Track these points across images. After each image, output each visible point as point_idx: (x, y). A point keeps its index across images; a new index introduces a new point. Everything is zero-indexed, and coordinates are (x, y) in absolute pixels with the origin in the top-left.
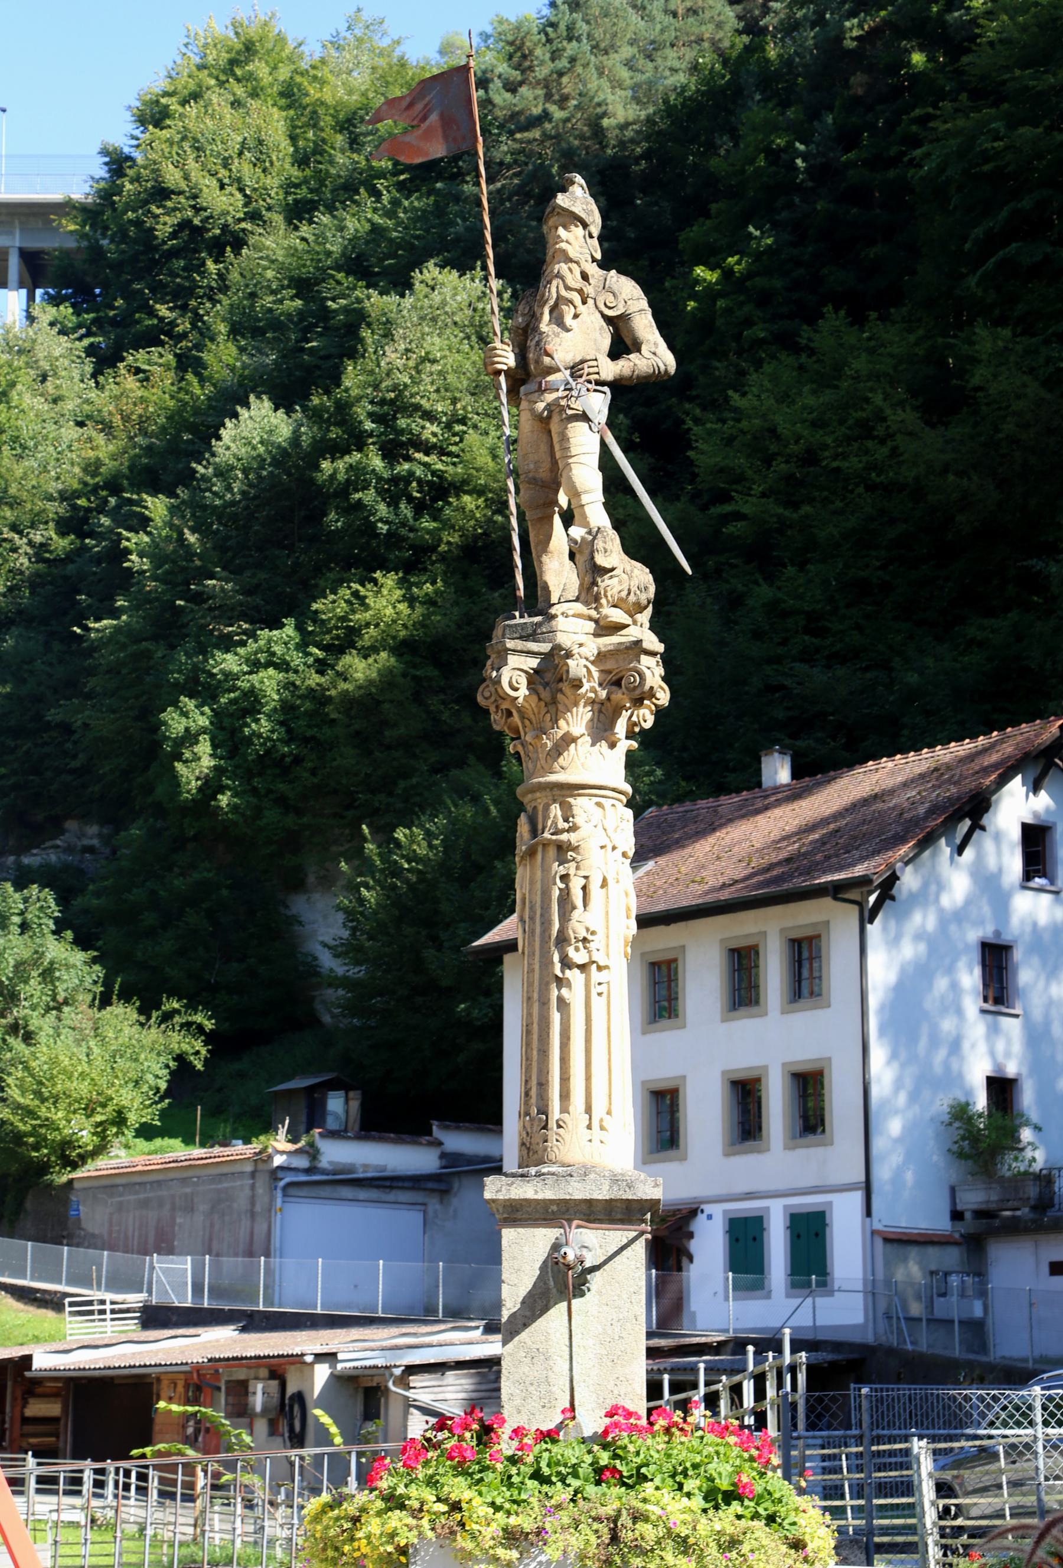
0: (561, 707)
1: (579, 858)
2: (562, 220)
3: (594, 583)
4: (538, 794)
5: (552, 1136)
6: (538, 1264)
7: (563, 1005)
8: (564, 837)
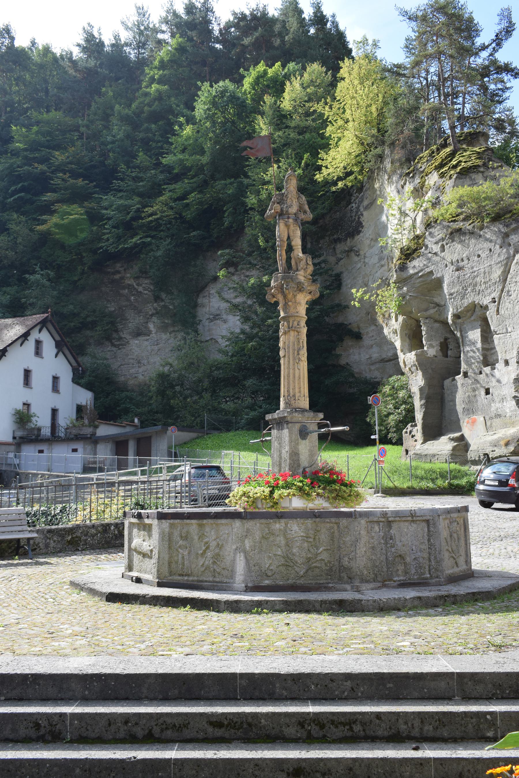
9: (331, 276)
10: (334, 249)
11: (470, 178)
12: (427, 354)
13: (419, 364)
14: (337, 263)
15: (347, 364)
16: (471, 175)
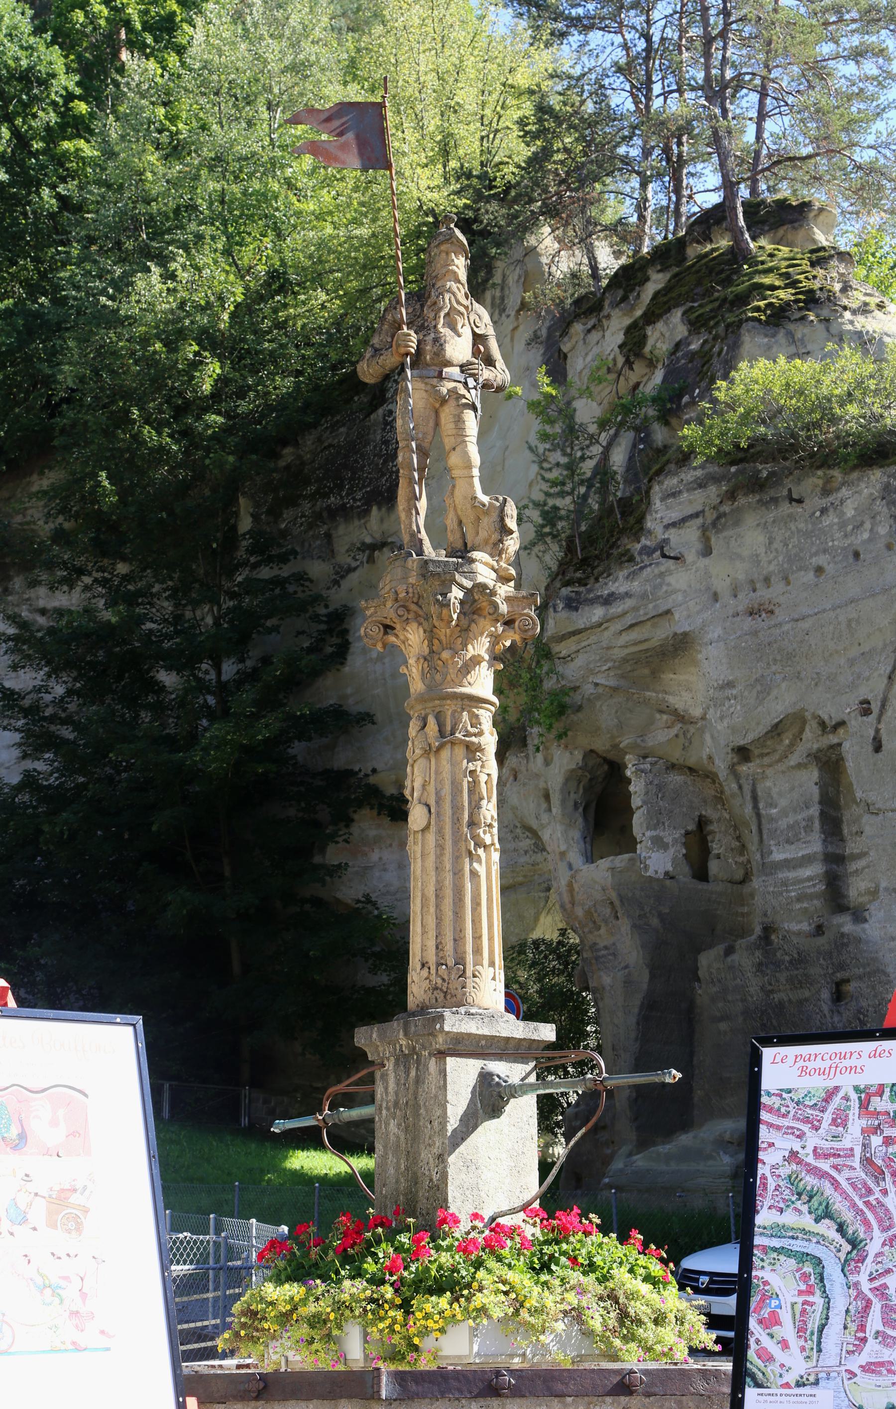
0: (471, 634)
1: (484, 759)
2: (454, 248)
3: (501, 541)
4: (448, 702)
5: (470, 982)
6: (470, 1089)
7: (474, 874)
8: (473, 739)
9: (316, 618)
10: (328, 536)
11: (790, 335)
12: (646, 867)
13: (621, 898)
14: (336, 583)
15: (368, 899)
16: (791, 327)
